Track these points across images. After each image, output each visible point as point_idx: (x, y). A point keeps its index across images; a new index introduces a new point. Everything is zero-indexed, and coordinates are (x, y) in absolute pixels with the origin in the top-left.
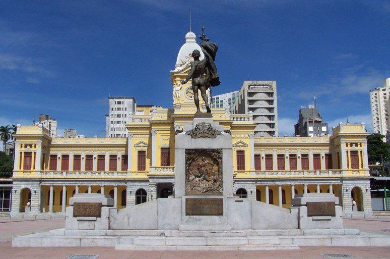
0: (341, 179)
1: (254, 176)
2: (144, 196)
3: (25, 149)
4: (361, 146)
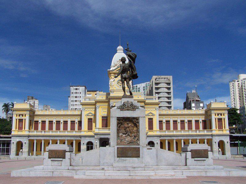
0: (212, 135)
3: (19, 117)
4: (224, 115)
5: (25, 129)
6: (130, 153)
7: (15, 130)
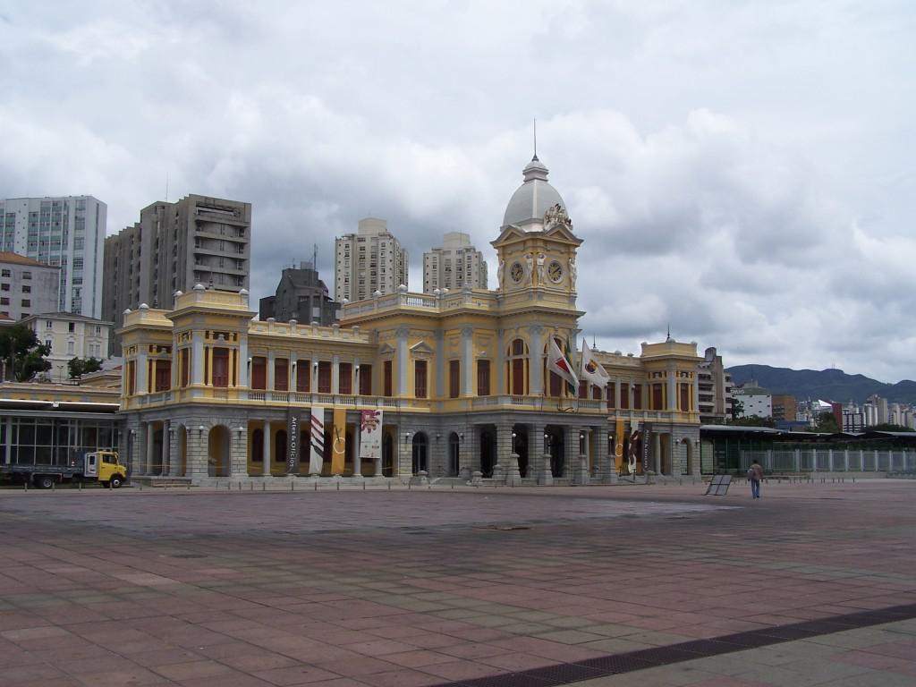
0: (672, 425)
1: (244, 400)
2: (423, 444)
3: (214, 341)
4: (235, 339)
5: (234, 385)
6: (640, 463)
7: (506, 394)
